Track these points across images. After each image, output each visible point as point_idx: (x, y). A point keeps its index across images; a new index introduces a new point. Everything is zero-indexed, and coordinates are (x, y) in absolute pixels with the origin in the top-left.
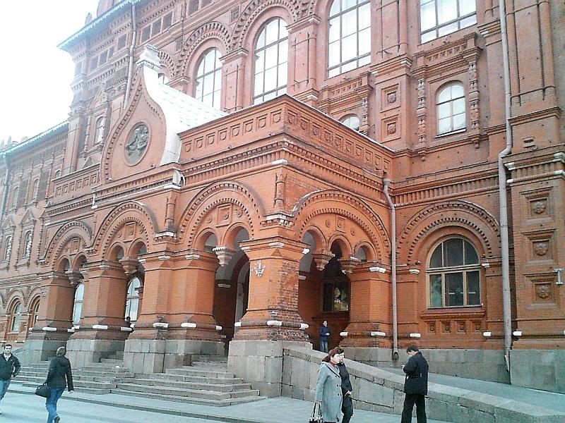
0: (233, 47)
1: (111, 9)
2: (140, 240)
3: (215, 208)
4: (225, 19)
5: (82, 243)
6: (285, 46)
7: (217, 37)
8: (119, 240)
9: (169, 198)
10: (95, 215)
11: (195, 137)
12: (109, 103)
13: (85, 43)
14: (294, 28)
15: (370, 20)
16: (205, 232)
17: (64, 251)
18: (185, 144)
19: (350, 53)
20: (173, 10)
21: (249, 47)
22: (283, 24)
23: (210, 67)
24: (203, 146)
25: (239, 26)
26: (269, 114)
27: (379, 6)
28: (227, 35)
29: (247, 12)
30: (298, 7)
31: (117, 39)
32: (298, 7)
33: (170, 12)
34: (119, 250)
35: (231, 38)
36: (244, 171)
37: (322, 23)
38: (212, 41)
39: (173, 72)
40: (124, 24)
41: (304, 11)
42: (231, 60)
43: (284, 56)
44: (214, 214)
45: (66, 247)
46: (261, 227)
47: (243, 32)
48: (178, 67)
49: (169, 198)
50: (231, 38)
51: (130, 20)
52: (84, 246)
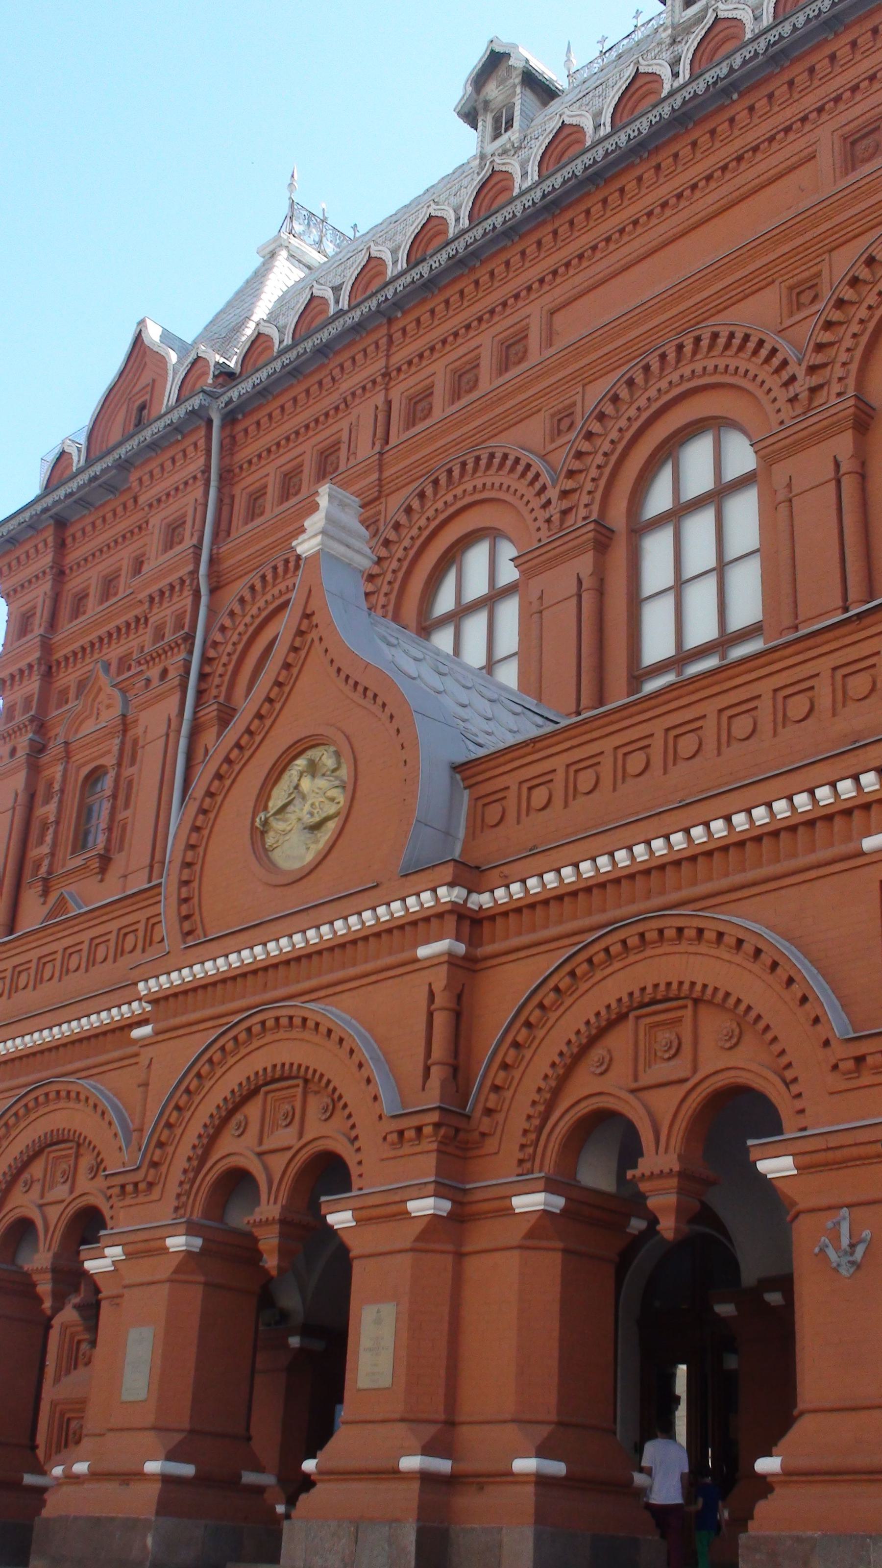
0: (562, 521)
1: (132, 437)
2: (321, 1145)
3: (622, 1017)
4: (528, 438)
5: (86, 1162)
6: (509, 613)
7: (508, 497)
8: (236, 1149)
9: (438, 987)
10: (144, 1060)
11: (618, 740)
12: (125, 724)
13: (50, 540)
14: (769, 455)
15: (517, 638)
16: (585, 1108)
17: (20, 1187)
18: (481, 803)
19: (702, 629)
20: (344, 424)
21: (617, 518)
22: (507, 551)
23: (477, 585)
24: (558, 800)
25: (579, 455)
26: (826, 674)
27: (535, 607)
28: (538, 486)
29: (609, 409)
30: (549, 502)
31: (157, 521)
32: (549, 502)
33: (473, 344)
34: (237, 1183)
35: (553, 493)
36: (738, 879)
37: (613, 542)
38: (487, 508)
39: (542, 515)
40: (100, 539)
41: (565, 513)
42: (552, 563)
43: (509, 638)
44: (620, 1041)
45: (26, 1176)
46: (836, 1082)
47: (855, 328)
48: (565, 494)
49: (438, 987)
50: (553, 493)
51: (202, 461)
52: (96, 1169)
